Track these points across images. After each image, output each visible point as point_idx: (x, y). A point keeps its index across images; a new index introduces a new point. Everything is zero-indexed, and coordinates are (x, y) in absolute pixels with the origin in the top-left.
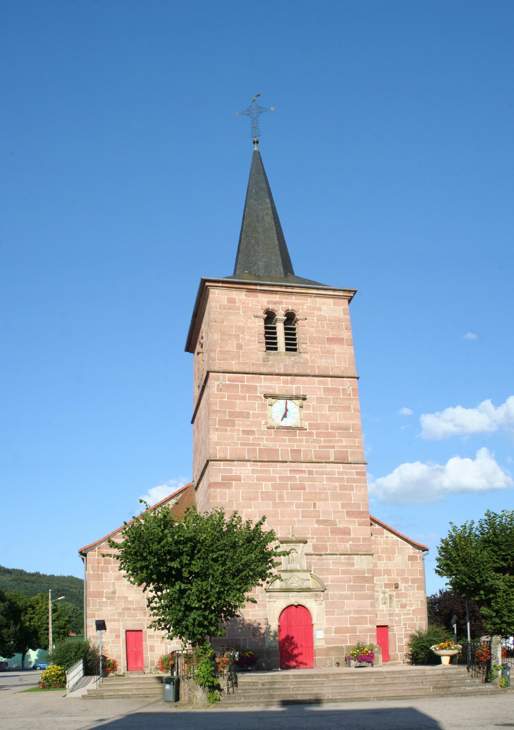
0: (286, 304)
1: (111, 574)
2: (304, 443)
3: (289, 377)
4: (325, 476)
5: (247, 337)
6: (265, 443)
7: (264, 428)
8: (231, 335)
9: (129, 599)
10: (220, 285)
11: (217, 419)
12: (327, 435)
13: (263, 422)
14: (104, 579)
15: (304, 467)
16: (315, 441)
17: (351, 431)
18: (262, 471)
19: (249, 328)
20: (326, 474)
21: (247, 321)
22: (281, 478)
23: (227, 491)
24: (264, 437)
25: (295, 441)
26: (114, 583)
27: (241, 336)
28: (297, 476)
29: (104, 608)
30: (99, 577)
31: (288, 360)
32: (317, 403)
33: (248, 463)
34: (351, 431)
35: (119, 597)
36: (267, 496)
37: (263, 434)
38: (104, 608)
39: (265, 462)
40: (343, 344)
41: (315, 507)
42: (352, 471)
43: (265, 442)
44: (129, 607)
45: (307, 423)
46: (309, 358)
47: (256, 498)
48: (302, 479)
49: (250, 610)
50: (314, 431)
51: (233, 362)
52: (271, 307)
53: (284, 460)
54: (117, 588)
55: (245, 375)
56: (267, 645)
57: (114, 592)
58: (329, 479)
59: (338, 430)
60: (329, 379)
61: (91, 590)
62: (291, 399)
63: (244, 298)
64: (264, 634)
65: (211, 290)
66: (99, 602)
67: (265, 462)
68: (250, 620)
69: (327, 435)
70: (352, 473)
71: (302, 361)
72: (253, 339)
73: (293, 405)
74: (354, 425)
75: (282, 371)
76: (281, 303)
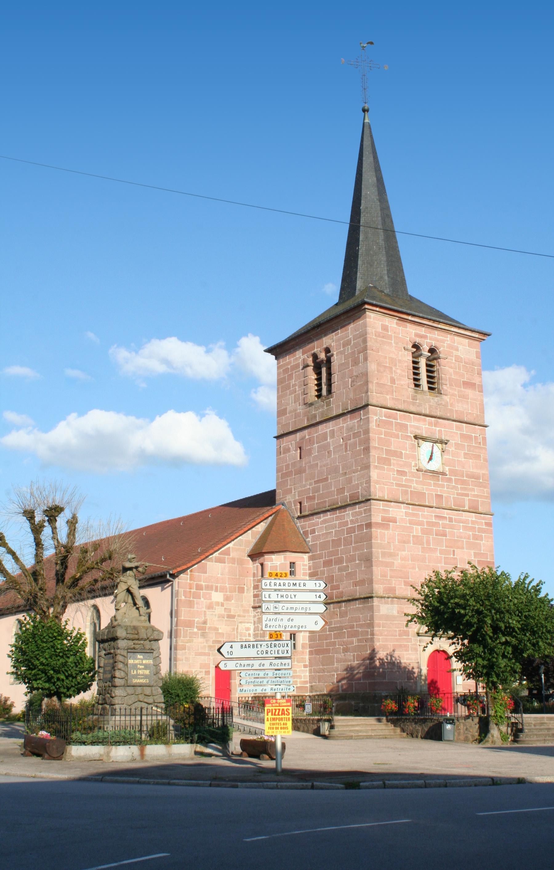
0: (431, 339)
1: (202, 602)
2: (445, 489)
3: (433, 419)
4: (461, 524)
5: (398, 371)
6: (415, 486)
7: (414, 469)
8: (385, 367)
9: (220, 631)
10: (378, 309)
11: (376, 456)
12: (463, 482)
13: (413, 464)
14: (195, 606)
15: (446, 513)
16: (454, 488)
17: (481, 481)
18: (414, 515)
19: (400, 361)
20: (462, 523)
21: (398, 353)
22: (429, 523)
23: (386, 532)
24: (415, 479)
25: (439, 486)
26: (205, 612)
27: (394, 369)
28: (441, 522)
29: (195, 640)
30: (191, 604)
31: (432, 401)
32: (455, 449)
33: (402, 505)
34: (481, 481)
35: (209, 628)
36: (418, 540)
37: (414, 477)
38: (195, 640)
39: (416, 505)
40: (475, 389)
41: (454, 555)
42: (482, 520)
43: (415, 485)
44: (220, 639)
45: (447, 469)
46: (448, 400)
47: (409, 542)
48: (444, 526)
49: (405, 653)
50: (453, 478)
51: (388, 397)
52: (418, 340)
53: (431, 505)
54: (208, 618)
55: (398, 412)
56: (419, 689)
57: (205, 622)
58: (465, 528)
59: (471, 478)
60: (464, 425)
61: (183, 618)
62: (436, 442)
63: (395, 326)
64: (416, 678)
65: (367, 313)
66: (190, 633)
67: (416, 505)
68: (405, 663)
69: (463, 482)
70: (482, 523)
71: (443, 403)
72: (403, 373)
73: (437, 448)
74: (483, 474)
75: (428, 412)
76: (425, 337)
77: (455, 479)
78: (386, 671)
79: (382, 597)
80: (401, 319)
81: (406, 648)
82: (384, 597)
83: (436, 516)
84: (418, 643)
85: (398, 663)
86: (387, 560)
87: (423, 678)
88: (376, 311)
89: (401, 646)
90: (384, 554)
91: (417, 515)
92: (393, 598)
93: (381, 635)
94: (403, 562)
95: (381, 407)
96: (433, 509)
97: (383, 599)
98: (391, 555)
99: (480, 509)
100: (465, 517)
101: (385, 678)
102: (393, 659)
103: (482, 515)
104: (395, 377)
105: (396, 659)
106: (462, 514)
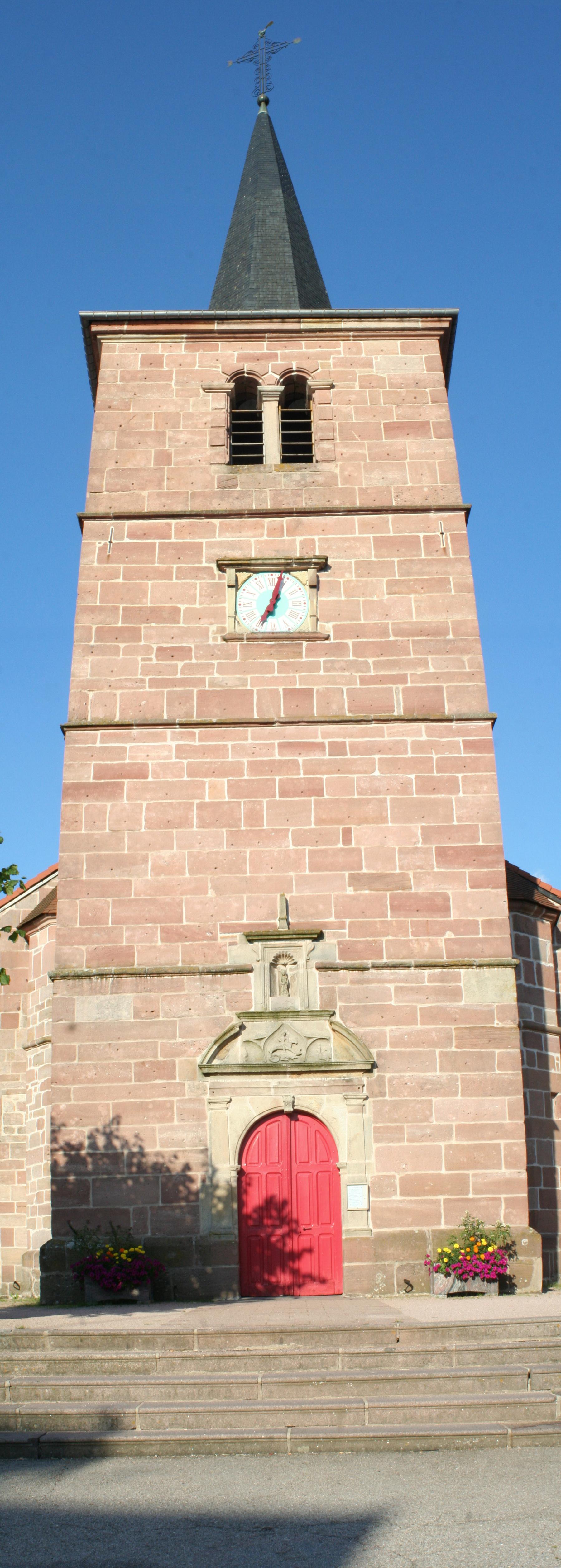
2: (322, 673)
4: (377, 757)
6: (217, 677)
10: (125, 328)
11: (94, 627)
12: (384, 649)
15: (319, 734)
16: (351, 665)
18: (204, 751)
28: (300, 760)
33: (169, 731)
36: (215, 815)
47: (184, 822)
49: (157, 1126)
53: (267, 717)
56: (204, 1226)
58: (390, 765)
64: (197, 1193)
68: (158, 1154)
70: (454, 747)
75: (269, 506)
77: (355, 645)
78: (90, 1179)
79: (78, 977)
80: (196, 336)
81: (163, 1112)
82: (89, 976)
83: (468, 745)
84: (207, 1097)
85: (132, 1155)
86: (107, 877)
87: (221, 1193)
88: (121, 332)
89: (142, 1108)
90: (95, 864)
91: (219, 751)
92: (119, 974)
93: (74, 1082)
94: (162, 877)
95: (117, 517)
96: (276, 728)
97: (86, 982)
98: (120, 863)
99: (448, 710)
100: (390, 735)
101: (84, 1199)
102: (117, 1143)
103: (454, 724)
104: (173, 450)
105: (125, 1144)
106: (382, 730)
